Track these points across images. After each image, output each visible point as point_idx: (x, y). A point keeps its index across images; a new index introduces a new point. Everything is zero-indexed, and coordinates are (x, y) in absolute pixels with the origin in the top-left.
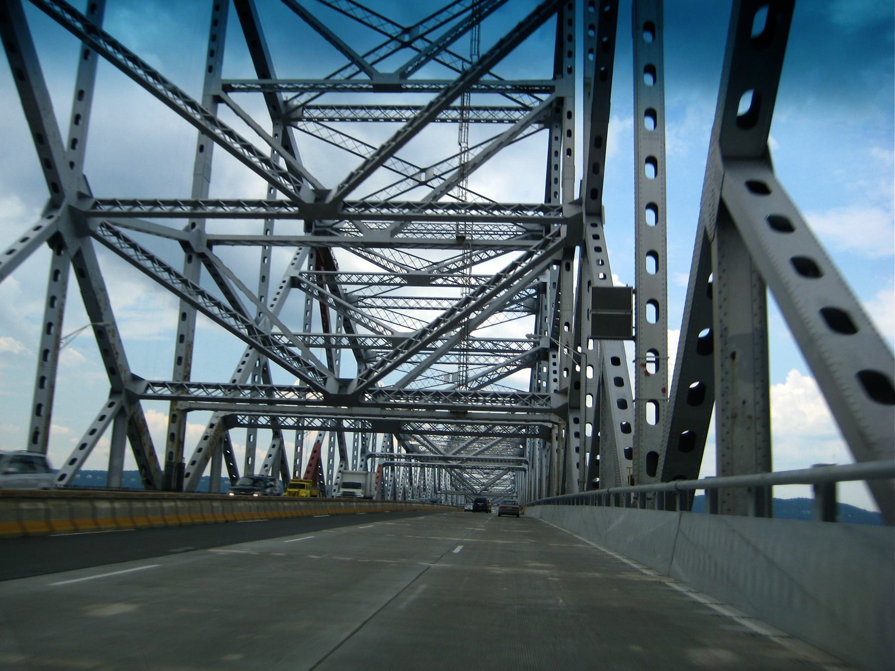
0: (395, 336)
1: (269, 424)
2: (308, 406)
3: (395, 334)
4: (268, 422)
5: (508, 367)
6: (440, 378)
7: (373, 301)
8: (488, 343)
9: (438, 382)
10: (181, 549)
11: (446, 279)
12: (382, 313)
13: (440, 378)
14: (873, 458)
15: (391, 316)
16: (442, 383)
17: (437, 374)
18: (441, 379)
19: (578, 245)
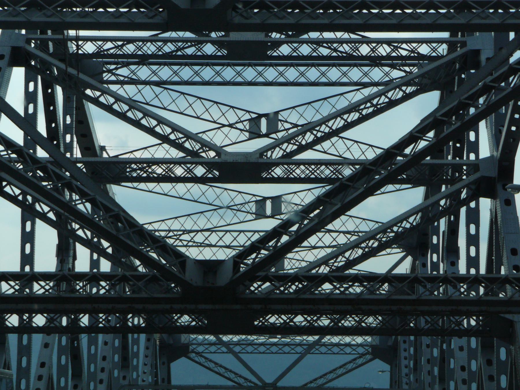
0: (224, 158)
1: (441, 208)
2: (70, 358)
3: (223, 156)
4: (443, 207)
5: (404, 88)
6: (247, 207)
7: (132, 72)
8: (384, 45)
9: (242, 216)
10: (362, 272)
11: (412, 51)
12: (148, 92)
13: (247, 207)
14: (9, 370)
15: (166, 97)
16: (250, 217)
17: (239, 200)
18: (249, 209)
19: (518, 103)
